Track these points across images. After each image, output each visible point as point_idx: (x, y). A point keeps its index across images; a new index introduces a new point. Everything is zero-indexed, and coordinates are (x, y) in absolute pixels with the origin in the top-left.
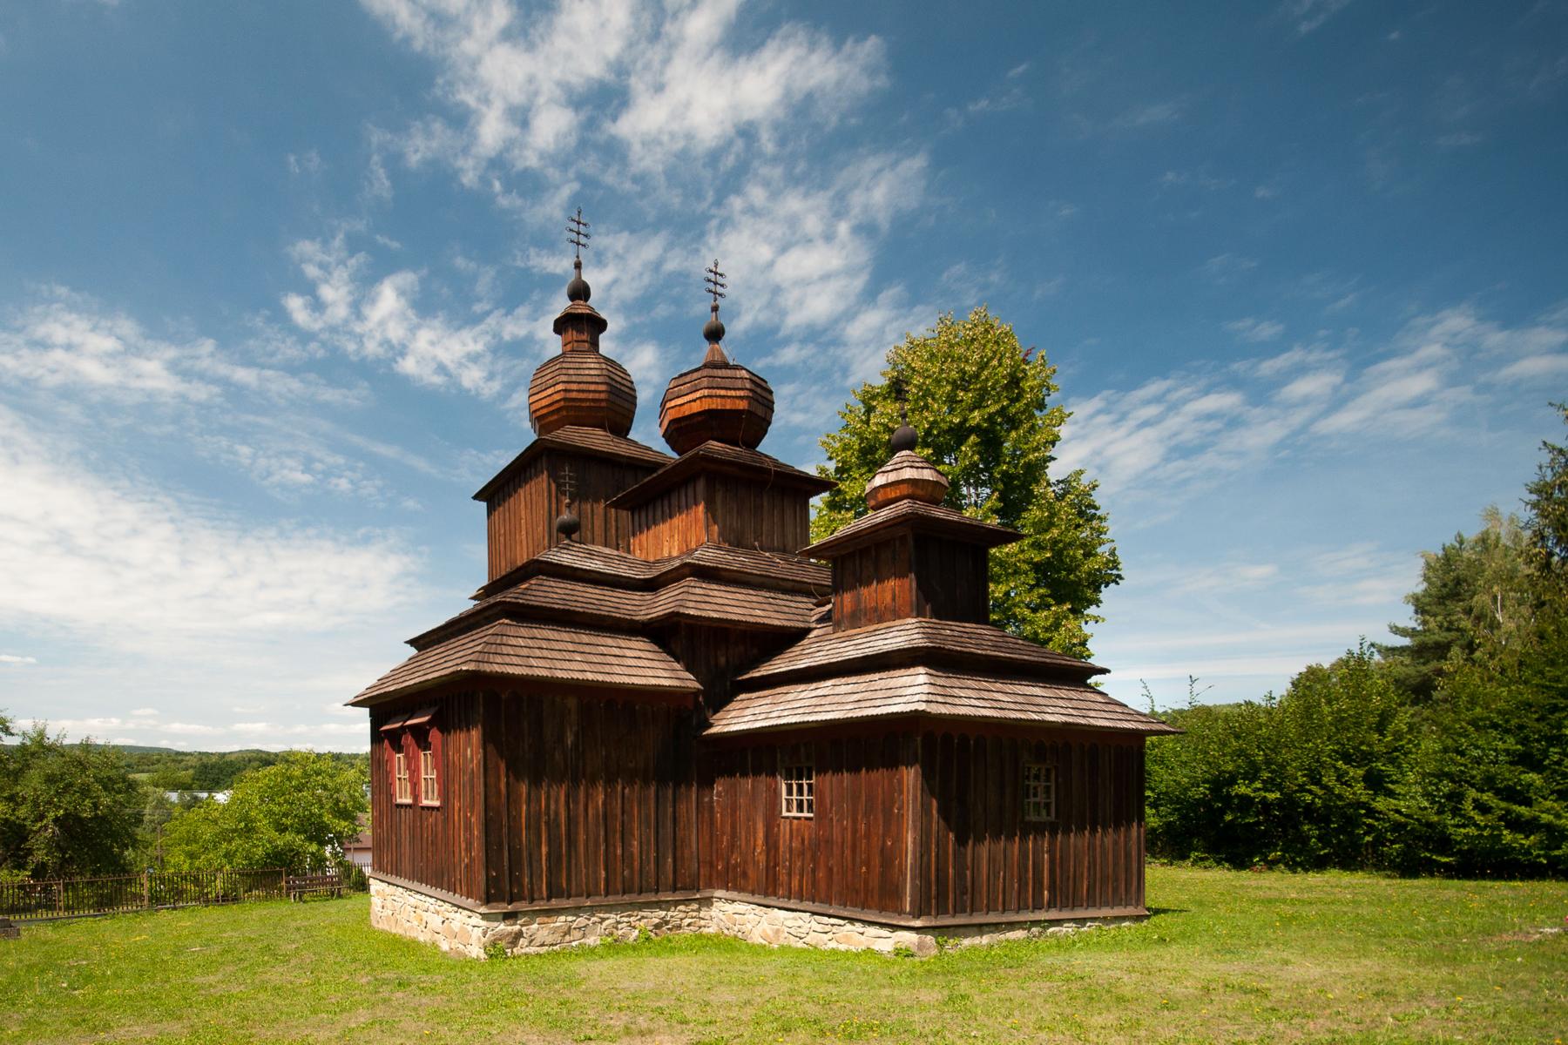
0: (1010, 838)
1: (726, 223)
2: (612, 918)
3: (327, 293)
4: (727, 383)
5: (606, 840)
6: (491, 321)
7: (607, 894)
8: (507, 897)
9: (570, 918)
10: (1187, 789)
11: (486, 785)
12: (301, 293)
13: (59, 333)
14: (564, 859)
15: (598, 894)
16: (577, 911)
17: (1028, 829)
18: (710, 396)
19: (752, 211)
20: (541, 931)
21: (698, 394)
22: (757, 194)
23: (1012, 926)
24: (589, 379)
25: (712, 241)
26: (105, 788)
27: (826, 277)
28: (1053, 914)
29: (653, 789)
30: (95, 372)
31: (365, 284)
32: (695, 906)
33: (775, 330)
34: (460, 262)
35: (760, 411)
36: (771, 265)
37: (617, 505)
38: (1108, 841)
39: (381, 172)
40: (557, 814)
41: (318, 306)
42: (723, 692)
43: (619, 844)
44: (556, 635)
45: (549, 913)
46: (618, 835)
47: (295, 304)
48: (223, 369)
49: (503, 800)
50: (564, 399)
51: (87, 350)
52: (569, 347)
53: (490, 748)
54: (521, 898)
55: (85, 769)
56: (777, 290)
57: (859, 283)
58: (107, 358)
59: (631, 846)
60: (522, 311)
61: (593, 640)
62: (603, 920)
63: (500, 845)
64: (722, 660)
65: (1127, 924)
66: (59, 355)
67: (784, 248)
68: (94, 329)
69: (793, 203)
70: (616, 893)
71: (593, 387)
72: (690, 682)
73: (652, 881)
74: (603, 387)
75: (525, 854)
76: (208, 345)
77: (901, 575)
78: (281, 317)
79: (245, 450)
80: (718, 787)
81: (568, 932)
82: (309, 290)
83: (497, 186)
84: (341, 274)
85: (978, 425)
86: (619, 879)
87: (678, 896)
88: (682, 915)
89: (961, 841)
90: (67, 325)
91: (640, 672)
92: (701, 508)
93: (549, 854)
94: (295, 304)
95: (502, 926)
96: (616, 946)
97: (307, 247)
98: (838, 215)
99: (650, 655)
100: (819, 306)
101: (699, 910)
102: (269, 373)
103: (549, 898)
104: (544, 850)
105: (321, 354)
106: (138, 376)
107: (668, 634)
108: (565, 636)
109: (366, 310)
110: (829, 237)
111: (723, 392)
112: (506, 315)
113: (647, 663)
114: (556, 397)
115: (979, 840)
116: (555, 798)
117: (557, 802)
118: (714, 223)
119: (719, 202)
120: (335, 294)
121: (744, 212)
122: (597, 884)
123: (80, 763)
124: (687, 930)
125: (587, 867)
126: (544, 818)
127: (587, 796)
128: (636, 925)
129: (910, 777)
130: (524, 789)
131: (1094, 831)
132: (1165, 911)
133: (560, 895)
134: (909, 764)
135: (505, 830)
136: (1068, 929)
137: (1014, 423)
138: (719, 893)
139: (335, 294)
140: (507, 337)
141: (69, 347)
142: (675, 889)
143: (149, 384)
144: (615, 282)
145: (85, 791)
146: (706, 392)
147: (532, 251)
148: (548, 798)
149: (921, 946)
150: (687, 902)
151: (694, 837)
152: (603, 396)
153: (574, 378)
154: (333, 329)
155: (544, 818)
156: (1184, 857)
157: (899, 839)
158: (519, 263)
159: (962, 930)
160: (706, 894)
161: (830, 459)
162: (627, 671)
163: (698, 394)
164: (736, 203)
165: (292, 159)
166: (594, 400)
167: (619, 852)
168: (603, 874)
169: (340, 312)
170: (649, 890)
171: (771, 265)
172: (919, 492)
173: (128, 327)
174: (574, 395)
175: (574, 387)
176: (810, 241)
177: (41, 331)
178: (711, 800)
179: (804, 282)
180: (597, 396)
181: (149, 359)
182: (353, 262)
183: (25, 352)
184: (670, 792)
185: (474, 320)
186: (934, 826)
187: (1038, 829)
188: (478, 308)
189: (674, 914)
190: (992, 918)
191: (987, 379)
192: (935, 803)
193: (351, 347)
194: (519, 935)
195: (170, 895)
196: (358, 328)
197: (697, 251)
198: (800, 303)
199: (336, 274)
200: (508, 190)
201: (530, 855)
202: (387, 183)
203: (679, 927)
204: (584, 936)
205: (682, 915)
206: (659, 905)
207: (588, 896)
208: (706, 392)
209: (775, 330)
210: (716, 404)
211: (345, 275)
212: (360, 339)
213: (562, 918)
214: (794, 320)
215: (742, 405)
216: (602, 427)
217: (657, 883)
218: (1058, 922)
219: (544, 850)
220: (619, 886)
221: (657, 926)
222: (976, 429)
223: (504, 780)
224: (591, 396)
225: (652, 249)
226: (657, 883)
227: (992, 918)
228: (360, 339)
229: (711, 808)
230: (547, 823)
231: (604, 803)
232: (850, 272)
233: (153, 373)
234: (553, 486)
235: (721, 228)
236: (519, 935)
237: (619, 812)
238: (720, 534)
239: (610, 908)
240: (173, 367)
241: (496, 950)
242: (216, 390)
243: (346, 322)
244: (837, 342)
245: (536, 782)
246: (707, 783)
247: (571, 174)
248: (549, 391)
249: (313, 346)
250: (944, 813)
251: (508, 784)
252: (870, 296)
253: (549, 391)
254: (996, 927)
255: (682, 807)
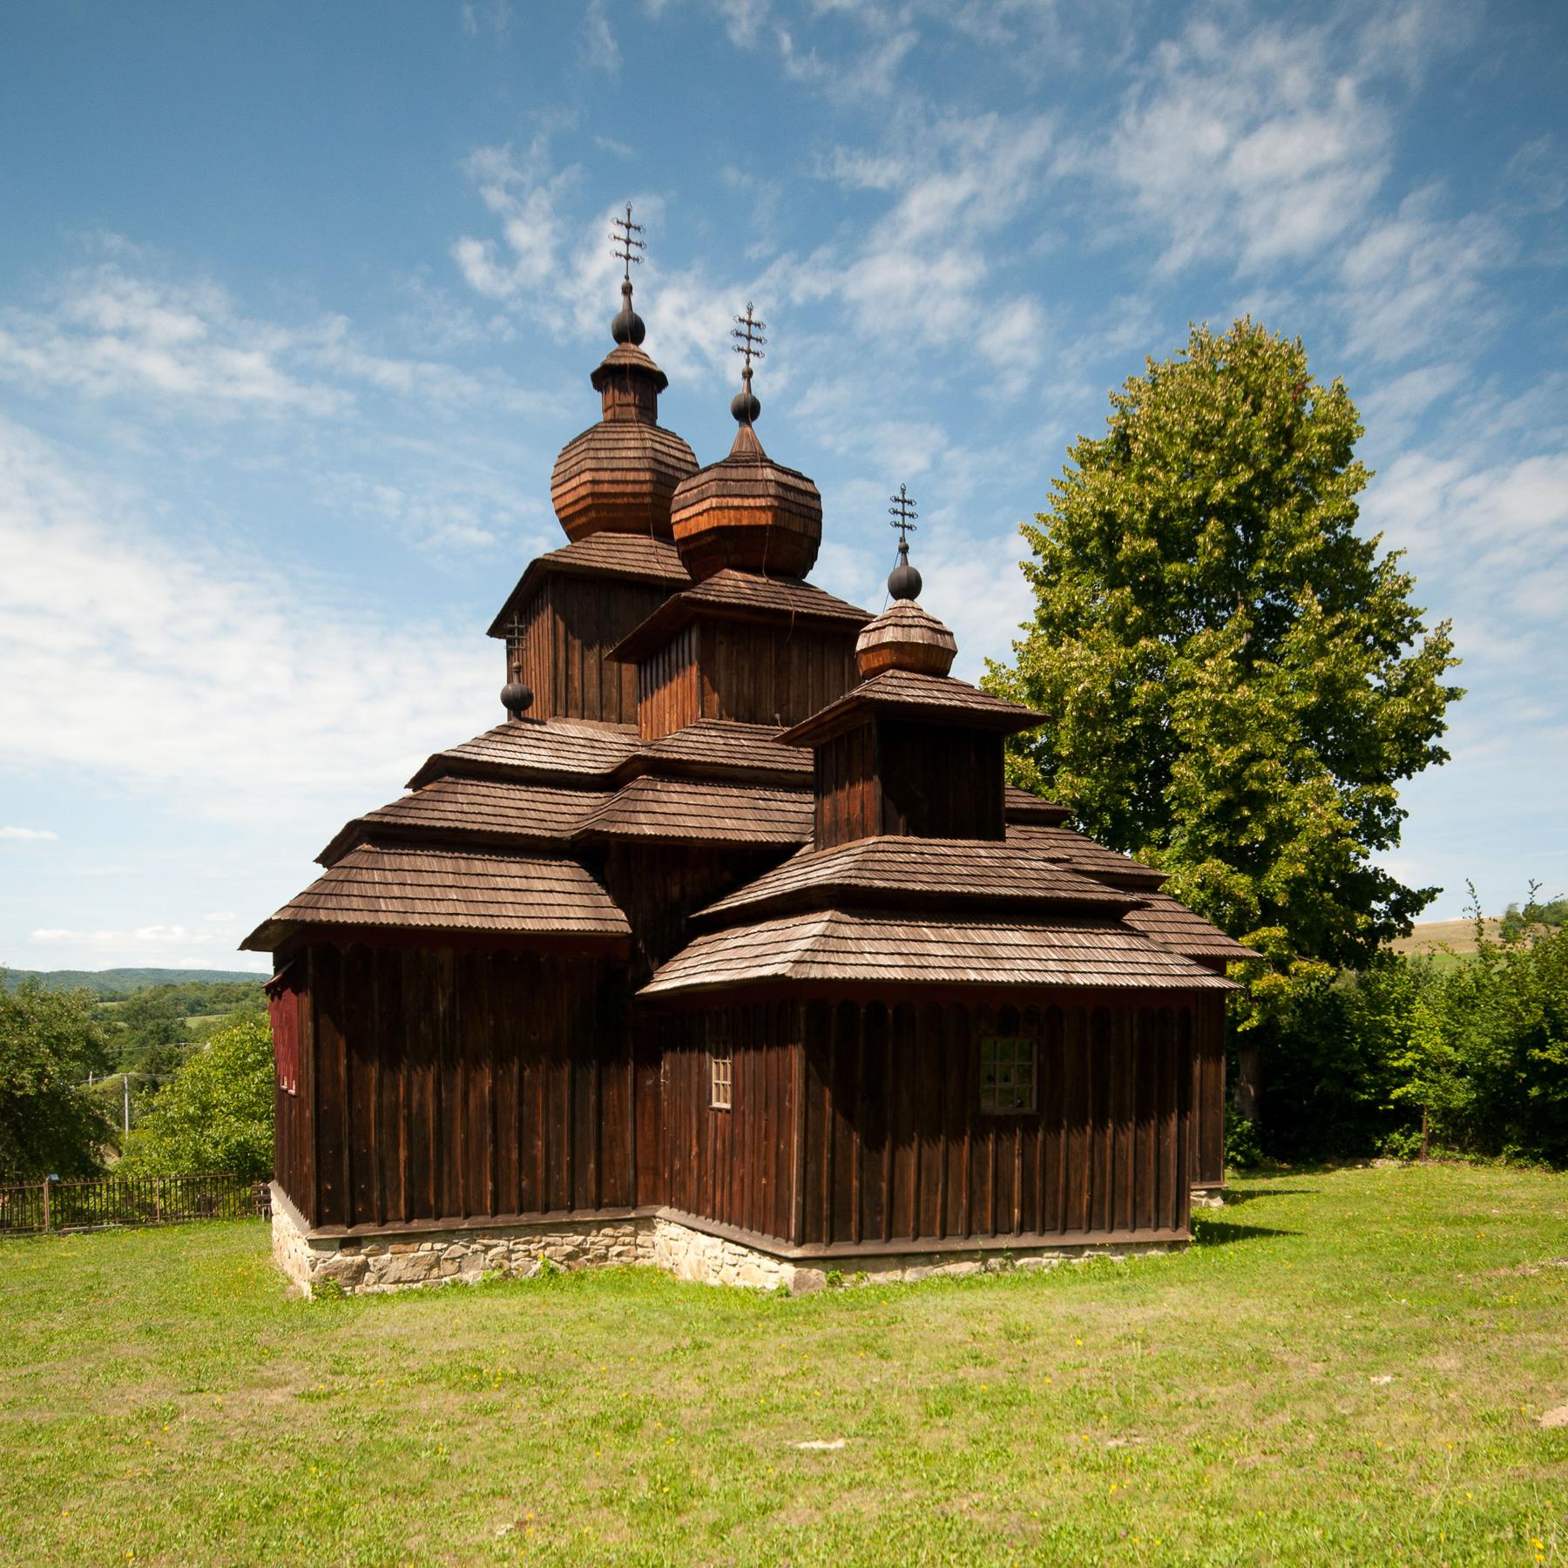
0: (956, 1137)
1: (1155, 91)
2: (502, 1246)
3: (521, 234)
4: (745, 488)
5: (495, 1141)
6: (776, 271)
7: (495, 1213)
8: (347, 1218)
9: (438, 1246)
10: (1486, 1054)
11: (317, 1069)
12: (479, 236)
13: (110, 312)
14: (432, 1165)
15: (482, 1212)
16: (449, 1235)
17: (984, 1126)
18: (720, 508)
19: (1196, 67)
20: (395, 1262)
21: (706, 505)
22: (1205, 37)
23: (956, 1256)
24: (626, 464)
25: (1129, 121)
26: (56, 1052)
27: (1314, 175)
28: (1029, 1240)
29: (567, 1070)
30: (161, 370)
31: (576, 220)
32: (629, 1229)
33: (1229, 268)
34: (731, 175)
35: (796, 526)
36: (1225, 156)
37: (621, 656)
38: (1127, 1139)
39: (603, 28)
40: (422, 1105)
41: (505, 256)
42: (671, 939)
43: (514, 1146)
44: (434, 864)
45: (407, 1238)
46: (513, 1134)
47: (471, 255)
48: (359, 365)
49: (343, 1089)
50: (592, 495)
51: (154, 340)
52: (610, 415)
53: (325, 1020)
54: (367, 1219)
55: (25, 1024)
56: (1233, 200)
57: (1371, 181)
58: (181, 351)
59: (533, 1147)
60: (823, 253)
61: (491, 868)
62: (488, 1248)
63: (339, 1152)
64: (675, 891)
65: (1154, 1253)
66: (109, 347)
67: (1250, 126)
68: (163, 304)
69: (1266, 50)
70: (510, 1211)
71: (631, 476)
72: (617, 921)
73: (564, 1194)
74: (647, 476)
75: (374, 1160)
76: (337, 325)
77: (867, 778)
78: (449, 275)
79: (391, 494)
80: (665, 1066)
81: (437, 1263)
82: (491, 228)
83: (786, 41)
84: (540, 201)
85: (1223, 502)
86: (514, 1192)
87: (603, 1215)
88: (608, 1241)
89: (873, 1143)
90: (121, 298)
91: (544, 912)
92: (694, 671)
93: (410, 1161)
94: (471, 255)
95: (338, 1257)
96: (507, 1279)
97: (489, 159)
98: (1339, 66)
99: (569, 887)
100: (1303, 222)
101: (635, 1234)
102: (429, 368)
103: (409, 1219)
104: (403, 1154)
105: (509, 335)
106: (231, 379)
107: (593, 853)
108: (448, 865)
109: (581, 262)
110: (1322, 104)
111: (737, 502)
112: (799, 262)
113: (560, 899)
114: (583, 491)
115: (900, 1142)
116: (420, 1086)
117: (422, 1089)
118: (1135, 90)
119: (1143, 55)
120: (530, 234)
121: (1182, 69)
122: (481, 1196)
123: (20, 1013)
124: (614, 1262)
125: (466, 1176)
126: (403, 1112)
127: (467, 1082)
128: (536, 1255)
129: (795, 1057)
130: (373, 1072)
131: (1100, 1125)
132: (1285, 1233)
133: (425, 1214)
134: (794, 1042)
135: (345, 1129)
136: (1052, 1260)
137: (1278, 496)
138: (664, 1211)
139: (530, 234)
140: (798, 298)
141: (124, 334)
142: (598, 1206)
143: (248, 391)
144: (973, 198)
145: (24, 1056)
146: (714, 502)
147: (839, 151)
148: (409, 1084)
149: (798, 1283)
150: (615, 1223)
151: (629, 1136)
152: (646, 488)
153: (605, 464)
154: (528, 295)
155: (403, 1112)
156: (1495, 1152)
157: (789, 1144)
158: (819, 174)
159: (870, 1262)
160: (645, 1212)
161: (1036, 553)
162: (522, 911)
163: (706, 505)
164: (1170, 54)
165: (468, 11)
166: (633, 495)
167: (515, 1156)
168: (490, 1186)
169: (542, 265)
170: (558, 1208)
171: (1225, 156)
172: (907, 660)
173: (214, 297)
174: (606, 488)
175: (606, 476)
176: (1292, 112)
177: (82, 308)
178: (657, 1084)
179: (1275, 185)
180: (637, 488)
181: (246, 350)
182: (559, 181)
183: (58, 343)
184: (593, 1073)
185: (747, 273)
186: (828, 1126)
187: (1003, 1125)
188: (753, 252)
189: (598, 1240)
190: (922, 1246)
191: (1236, 433)
192: (828, 1094)
193: (557, 323)
194: (364, 1268)
195: (137, 1211)
196: (566, 291)
197: (1105, 140)
198: (1271, 220)
199: (532, 202)
200: (802, 49)
201: (382, 1163)
202: (612, 46)
203: (605, 1257)
204: (460, 1270)
205: (608, 1241)
206: (573, 1227)
207: (467, 1216)
208: (714, 502)
209: (1229, 268)
210: (729, 519)
211: (546, 204)
212: (568, 308)
213: (428, 1246)
214: (1263, 249)
215: (765, 519)
216: (645, 532)
217: (572, 1198)
218: (1035, 1251)
219: (403, 1154)
220: (515, 1202)
221: (570, 1256)
222: (1220, 511)
223: (344, 1062)
224: (629, 489)
225: (1034, 139)
226: (572, 1198)
227: (922, 1246)
228: (568, 308)
229: (657, 1095)
230: (408, 1119)
231: (493, 1091)
232: (1355, 162)
233: (253, 373)
234: (561, 626)
235: (1145, 102)
236: (364, 1268)
237: (514, 1101)
238: (721, 705)
239: (498, 1232)
240: (283, 363)
241: (329, 1288)
242: (348, 397)
243: (550, 282)
244: (1329, 285)
245: (391, 1063)
246: (651, 1060)
247: (905, 16)
248: (574, 483)
249: (498, 322)
250: (845, 1106)
251: (349, 1067)
252: (1386, 204)
253: (574, 483)
254: (929, 1258)
255: (611, 1094)
